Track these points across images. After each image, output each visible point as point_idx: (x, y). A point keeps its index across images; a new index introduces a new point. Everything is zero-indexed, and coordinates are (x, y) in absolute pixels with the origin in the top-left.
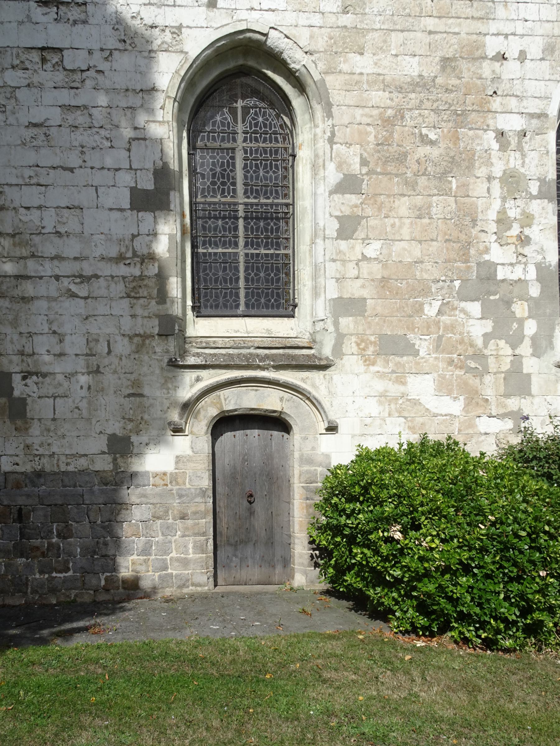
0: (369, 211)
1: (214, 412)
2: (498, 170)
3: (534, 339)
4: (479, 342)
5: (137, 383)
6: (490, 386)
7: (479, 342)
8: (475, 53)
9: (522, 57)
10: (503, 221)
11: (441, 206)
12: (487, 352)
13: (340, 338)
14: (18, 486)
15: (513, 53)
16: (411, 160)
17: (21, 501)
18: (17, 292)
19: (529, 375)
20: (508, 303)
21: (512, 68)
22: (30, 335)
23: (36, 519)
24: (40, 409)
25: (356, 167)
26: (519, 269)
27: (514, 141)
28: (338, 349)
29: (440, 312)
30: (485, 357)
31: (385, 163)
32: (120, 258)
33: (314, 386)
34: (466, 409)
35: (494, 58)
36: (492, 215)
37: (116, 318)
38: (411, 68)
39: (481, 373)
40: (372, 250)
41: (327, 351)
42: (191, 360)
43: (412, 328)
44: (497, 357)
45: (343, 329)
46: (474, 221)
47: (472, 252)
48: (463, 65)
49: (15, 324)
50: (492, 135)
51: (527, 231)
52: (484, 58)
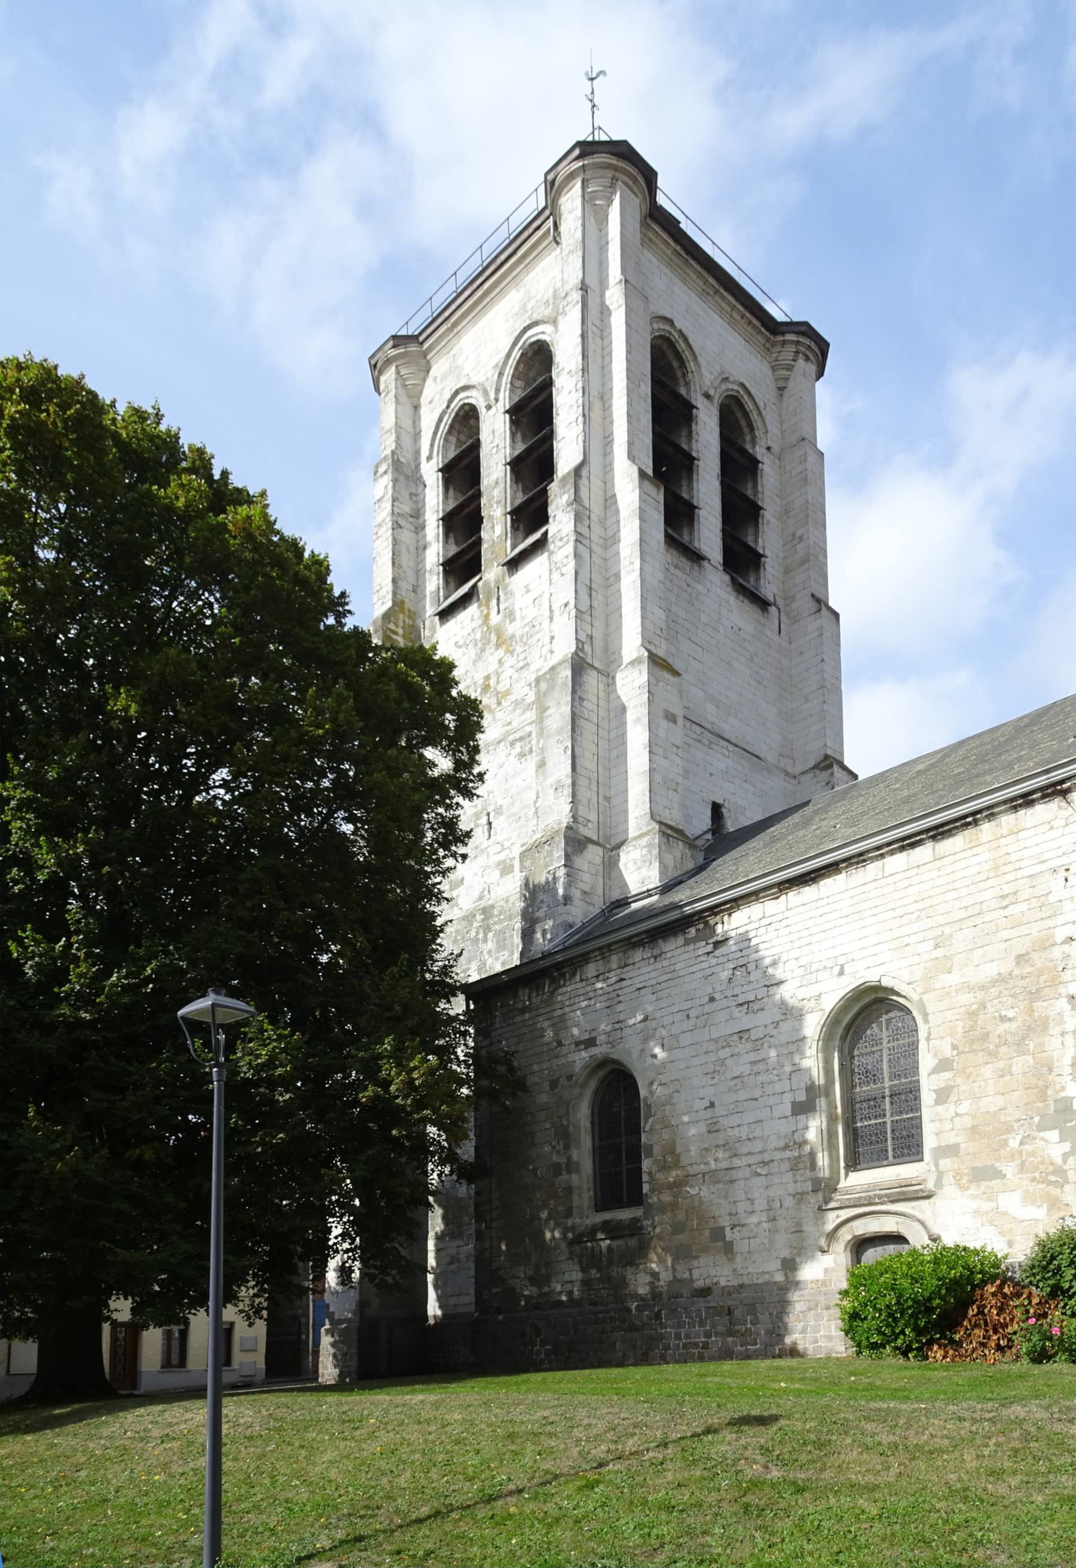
0: (959, 1081)
1: (849, 1237)
5: (798, 1224)
11: (1021, 1064)
12: (1066, 1167)
14: (730, 1294)
16: (994, 1038)
17: (730, 1303)
18: (728, 1178)
22: (735, 1202)
23: (738, 1313)
24: (741, 1247)
25: (948, 1052)
29: (1021, 1143)
30: (1065, 1172)
32: (786, 1147)
33: (921, 1211)
35: (1064, 943)
37: (785, 1184)
38: (991, 971)
41: (930, 1185)
43: (998, 1159)
46: (1050, 1070)
47: (1050, 1092)
48: (1035, 956)
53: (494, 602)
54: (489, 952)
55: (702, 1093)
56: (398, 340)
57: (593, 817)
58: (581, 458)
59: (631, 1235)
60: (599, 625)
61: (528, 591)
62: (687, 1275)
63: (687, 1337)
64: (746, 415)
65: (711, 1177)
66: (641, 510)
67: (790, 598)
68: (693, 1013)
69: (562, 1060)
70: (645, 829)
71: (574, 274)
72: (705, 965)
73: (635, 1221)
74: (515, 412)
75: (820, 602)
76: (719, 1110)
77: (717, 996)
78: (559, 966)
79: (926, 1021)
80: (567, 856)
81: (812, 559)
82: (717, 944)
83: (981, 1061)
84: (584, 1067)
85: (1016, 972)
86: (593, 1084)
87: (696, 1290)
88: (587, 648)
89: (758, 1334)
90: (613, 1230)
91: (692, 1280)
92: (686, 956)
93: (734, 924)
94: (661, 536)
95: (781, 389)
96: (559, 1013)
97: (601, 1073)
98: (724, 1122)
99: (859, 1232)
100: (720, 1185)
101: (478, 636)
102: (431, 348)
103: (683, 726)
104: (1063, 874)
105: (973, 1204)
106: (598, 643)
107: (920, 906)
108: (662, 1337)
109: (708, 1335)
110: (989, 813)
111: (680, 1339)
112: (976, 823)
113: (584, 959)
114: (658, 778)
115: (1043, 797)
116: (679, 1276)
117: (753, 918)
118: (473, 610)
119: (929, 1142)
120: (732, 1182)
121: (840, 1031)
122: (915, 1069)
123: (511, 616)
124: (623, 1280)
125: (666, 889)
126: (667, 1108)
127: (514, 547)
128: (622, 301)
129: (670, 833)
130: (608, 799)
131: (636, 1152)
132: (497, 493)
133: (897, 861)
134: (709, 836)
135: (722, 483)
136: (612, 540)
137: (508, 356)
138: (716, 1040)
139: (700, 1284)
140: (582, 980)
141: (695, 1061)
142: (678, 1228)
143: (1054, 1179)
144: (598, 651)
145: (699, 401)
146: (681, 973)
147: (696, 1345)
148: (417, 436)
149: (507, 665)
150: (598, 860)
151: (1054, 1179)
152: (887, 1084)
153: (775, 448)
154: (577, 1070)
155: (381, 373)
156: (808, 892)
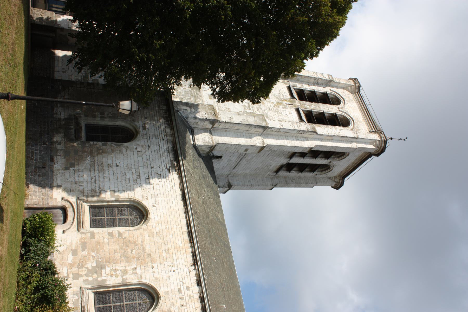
0: (115, 239)
1: (67, 206)
2: (127, 268)
3: (88, 280)
4: (86, 266)
5: (73, 191)
6: (75, 269)
7: (86, 266)
8: (152, 261)
9: (154, 272)
10: (116, 270)
11: (118, 255)
12: (84, 268)
13: (85, 233)
14: (50, 168)
15: (154, 270)
16: (127, 248)
17: (47, 168)
18: (92, 169)
19: (78, 279)
20: (96, 273)
21: (151, 270)
22: (83, 171)
23: (43, 170)
24: (67, 172)
25: (124, 236)
26: (105, 275)
27: (134, 271)
28: (82, 233)
29: (93, 256)
30: (82, 268)
31: (126, 242)
32: (100, 188)
33: (74, 228)
34: (69, 264)
35: (152, 266)
36: (117, 268)
37: (87, 187)
38: (147, 247)
39: (78, 267)
40: (106, 240)
41: (82, 230)
42: (78, 201)
43: (88, 250)
44: (82, 271)
45: (87, 234)
46: (115, 263)
47: (108, 263)
48: (150, 259)
49: (85, 168)
50: (135, 266)
51: (114, 276)
52: (152, 263)
53: (289, 103)
54: (185, 88)
55: (122, 163)
56: (359, 87)
57: (221, 127)
58: (345, 179)
59: (75, 137)
60: (276, 133)
61: (290, 113)
62: (59, 154)
63: (36, 153)
64: (325, 170)
65: (93, 164)
66: (303, 147)
67: (278, 178)
68: (148, 162)
69: (140, 119)
70: (214, 141)
71: (361, 136)
72: (163, 166)
73: (81, 137)
74: (335, 115)
75: (275, 186)
76: (115, 168)
77: (153, 169)
78: (171, 120)
79: (135, 230)
80: (209, 120)
81: (287, 183)
82: (169, 170)
83: (120, 245)
84: (136, 125)
85: (146, 254)
86: (131, 127)
87: (53, 157)
88: (269, 130)
89: (35, 177)
90: (78, 131)
91: (57, 156)
92: (167, 160)
93: (174, 176)
94: (296, 151)
95: (330, 178)
96: (156, 118)
97: (134, 130)
98: (111, 170)
99: (68, 209)
100: (89, 167)
101: (281, 97)
102: (356, 95)
103: (244, 153)
104: (172, 265)
105: (74, 243)
106: (271, 133)
107: (170, 228)
108: (36, 144)
109: (36, 160)
110: (193, 246)
111: (35, 151)
112: (191, 243)
113: (172, 129)
114: (229, 146)
115: (194, 260)
116: (59, 151)
117: (175, 181)
118: (289, 96)
119: (96, 230)
120: (90, 171)
121: (136, 205)
122: (120, 226)
123: (284, 107)
124: (60, 133)
125: (195, 146)
126: (118, 152)
127: (303, 110)
128: (353, 147)
129: (212, 148)
130: (226, 131)
131: (105, 139)
132: (317, 108)
133: (184, 222)
134: (212, 155)
135: (309, 164)
136: (297, 139)
137: (349, 115)
138: (138, 168)
139: (55, 158)
140: (165, 127)
141: (132, 161)
142: (76, 152)
143: (80, 265)
144: (268, 132)
145: (329, 160)
146: (162, 159)
147: (32, 156)
148: (337, 87)
149: (271, 104)
150: (207, 127)
151: (80, 265)
152: (117, 217)
153: (316, 176)
154: (136, 123)
155: (353, 81)
156: (180, 197)
